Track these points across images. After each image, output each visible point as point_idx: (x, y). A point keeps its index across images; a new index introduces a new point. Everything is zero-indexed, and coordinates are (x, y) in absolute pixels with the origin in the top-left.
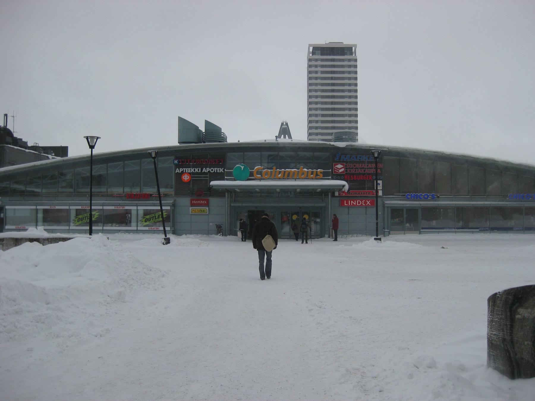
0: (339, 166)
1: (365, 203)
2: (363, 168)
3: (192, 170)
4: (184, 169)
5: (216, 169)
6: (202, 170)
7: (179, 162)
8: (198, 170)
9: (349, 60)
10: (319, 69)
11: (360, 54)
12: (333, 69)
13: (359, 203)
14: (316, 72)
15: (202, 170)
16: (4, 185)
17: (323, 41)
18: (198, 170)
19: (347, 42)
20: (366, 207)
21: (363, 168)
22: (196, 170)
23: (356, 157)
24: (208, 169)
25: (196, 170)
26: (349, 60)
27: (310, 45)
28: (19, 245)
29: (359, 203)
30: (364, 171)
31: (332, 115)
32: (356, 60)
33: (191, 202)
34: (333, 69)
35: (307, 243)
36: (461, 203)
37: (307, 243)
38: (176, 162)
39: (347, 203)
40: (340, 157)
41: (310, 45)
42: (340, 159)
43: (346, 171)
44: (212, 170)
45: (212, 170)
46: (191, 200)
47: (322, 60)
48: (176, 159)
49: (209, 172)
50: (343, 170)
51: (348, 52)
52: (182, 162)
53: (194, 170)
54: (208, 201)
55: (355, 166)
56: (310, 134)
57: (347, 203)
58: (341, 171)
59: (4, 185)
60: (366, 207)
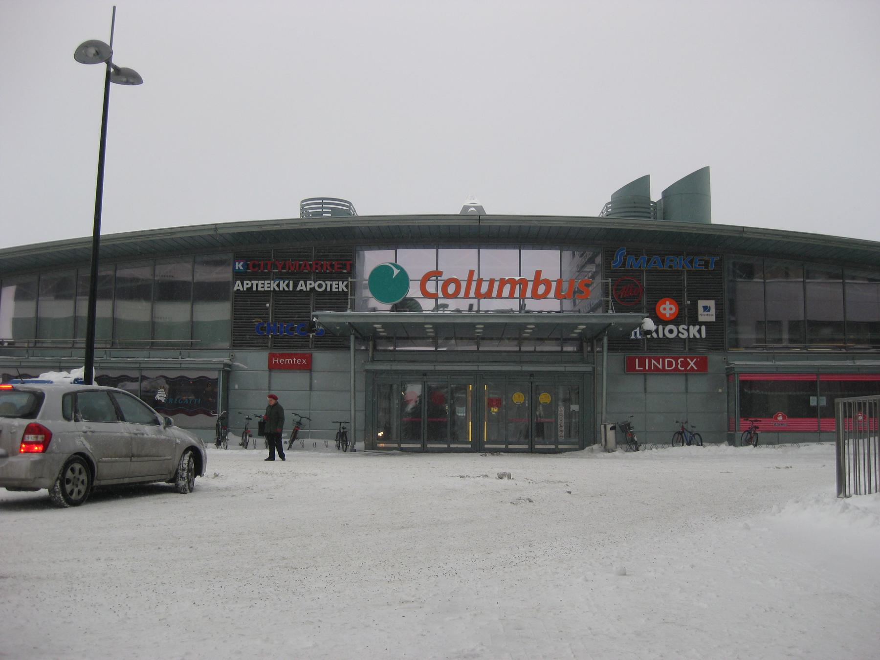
1: (685, 364)
4: (255, 282)
6: (295, 286)
7: (246, 266)
13: (670, 364)
15: (295, 286)
16: (870, 363)
18: (288, 285)
20: (645, 375)
23: (663, 261)
24: (311, 284)
25: (283, 285)
28: (752, 439)
29: (670, 364)
33: (270, 361)
35: (282, 457)
37: (282, 457)
38: (239, 266)
39: (642, 364)
40: (625, 260)
42: (624, 265)
44: (320, 286)
46: (271, 356)
48: (238, 258)
49: (313, 289)
52: (254, 266)
53: (278, 285)
54: (309, 359)
57: (642, 364)
59: (870, 363)
60: (645, 375)
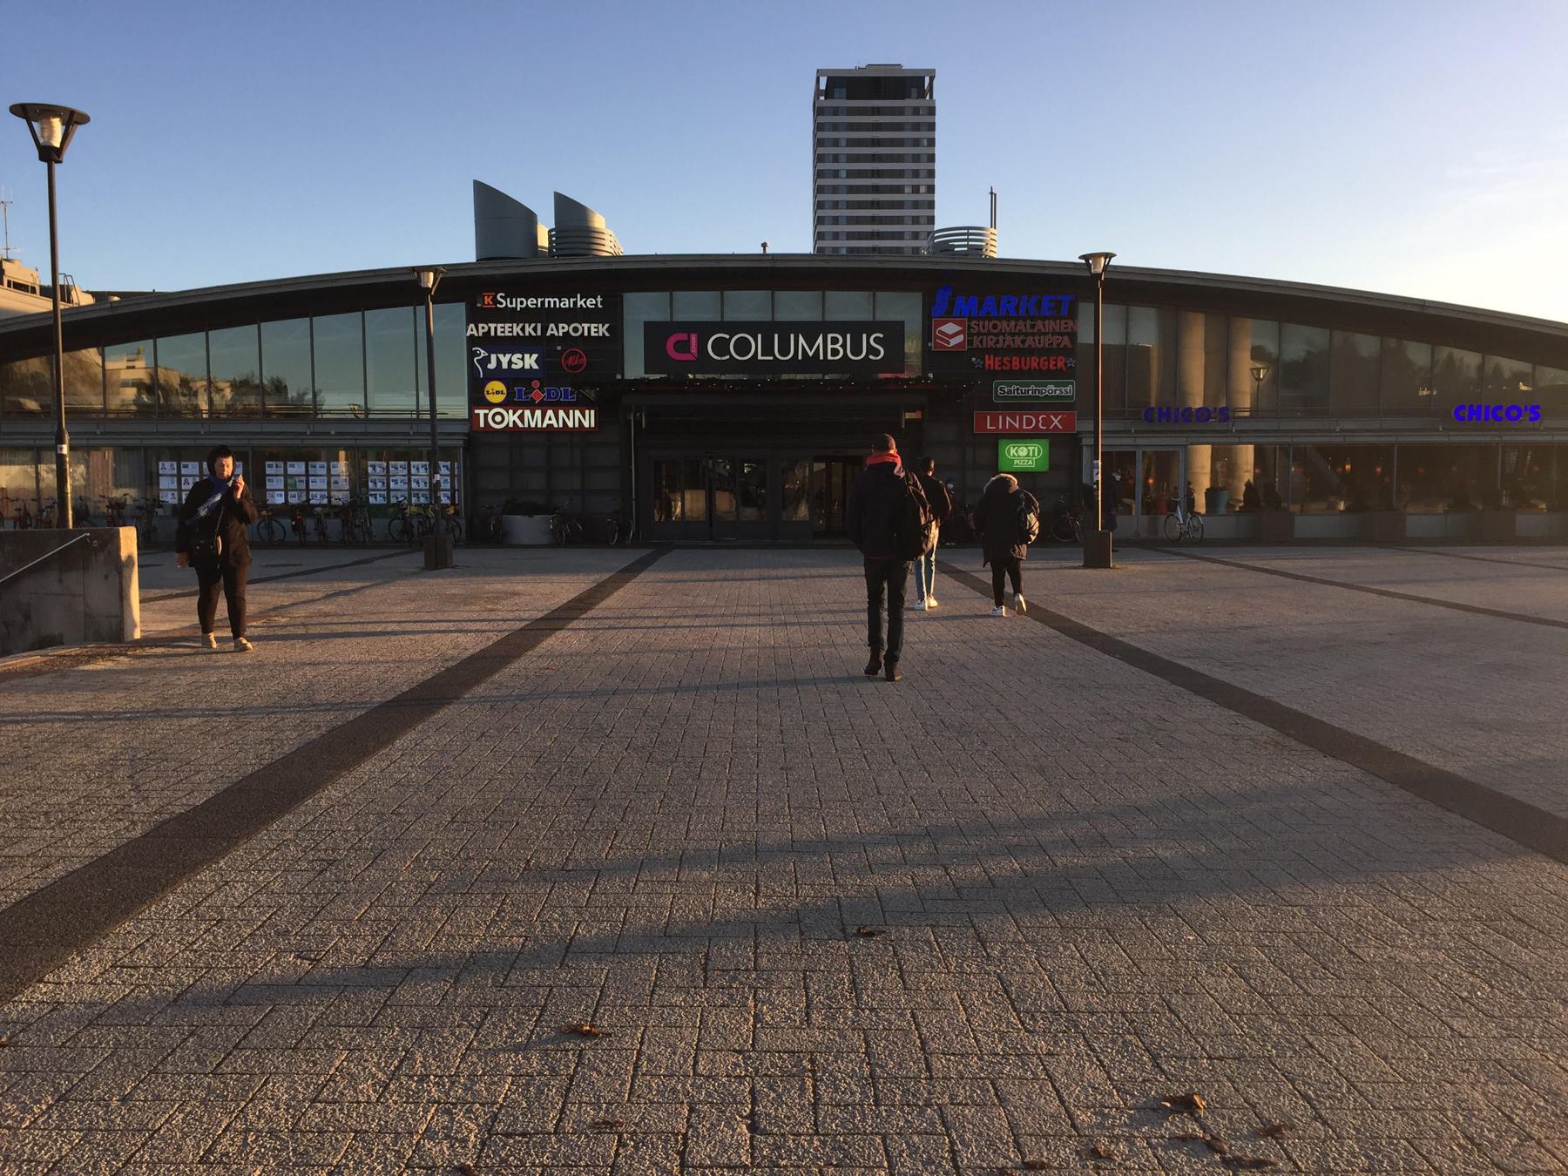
0: (950, 328)
2: (1020, 334)
3: (517, 329)
4: (492, 326)
5: (586, 326)
8: (535, 329)
9: (916, 111)
10: (843, 166)
11: (942, 96)
12: (875, 119)
14: (836, 174)
15: (544, 329)
17: (851, 59)
18: (535, 329)
19: (910, 60)
21: (1020, 334)
22: (529, 330)
25: (529, 330)
26: (916, 111)
27: (820, 73)
30: (1023, 342)
31: (874, 220)
32: (932, 111)
34: (875, 119)
36: (1382, 439)
41: (820, 73)
43: (970, 342)
44: (576, 330)
45: (576, 330)
47: (851, 111)
50: (960, 338)
51: (914, 91)
53: (523, 329)
55: (995, 327)
56: (819, 236)
58: (954, 342)
